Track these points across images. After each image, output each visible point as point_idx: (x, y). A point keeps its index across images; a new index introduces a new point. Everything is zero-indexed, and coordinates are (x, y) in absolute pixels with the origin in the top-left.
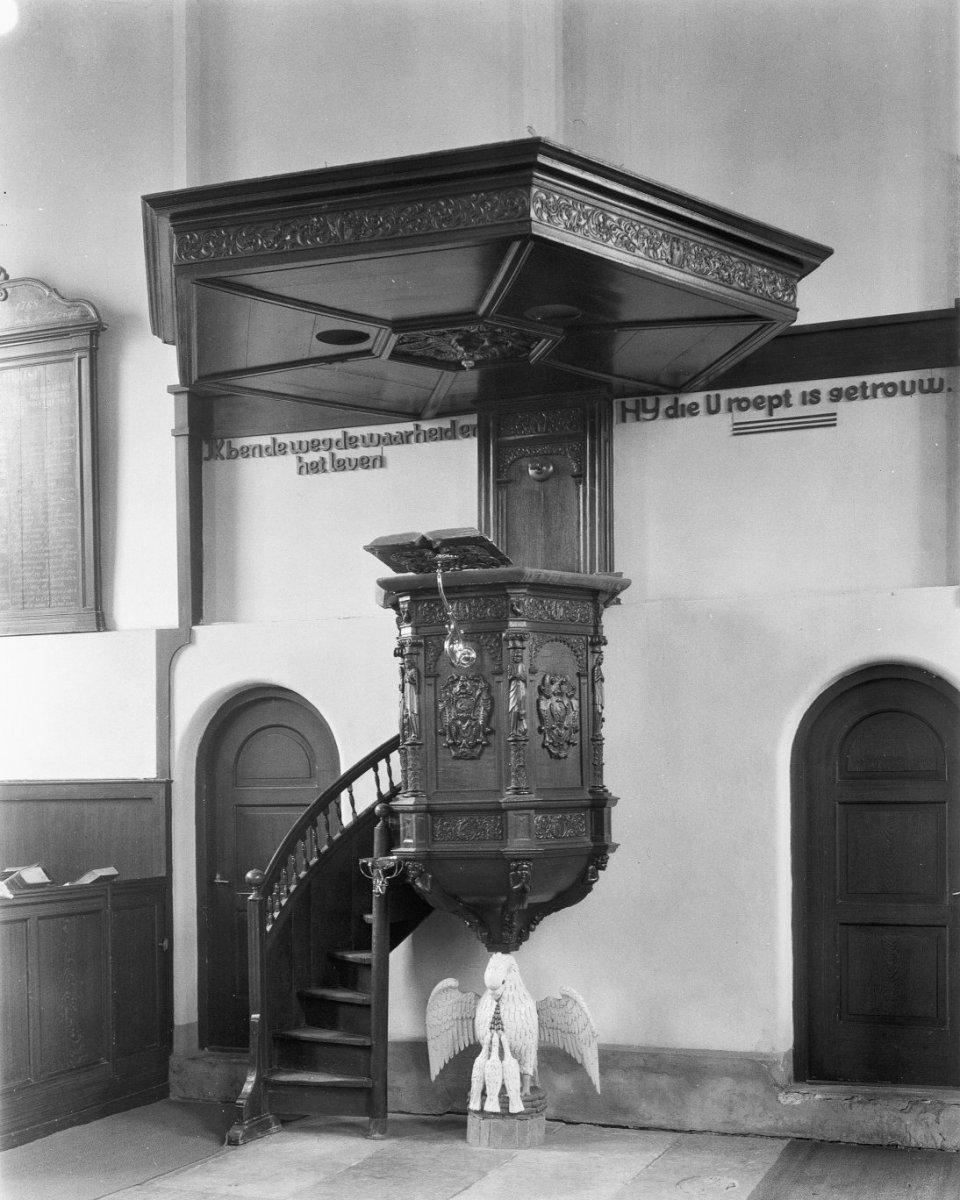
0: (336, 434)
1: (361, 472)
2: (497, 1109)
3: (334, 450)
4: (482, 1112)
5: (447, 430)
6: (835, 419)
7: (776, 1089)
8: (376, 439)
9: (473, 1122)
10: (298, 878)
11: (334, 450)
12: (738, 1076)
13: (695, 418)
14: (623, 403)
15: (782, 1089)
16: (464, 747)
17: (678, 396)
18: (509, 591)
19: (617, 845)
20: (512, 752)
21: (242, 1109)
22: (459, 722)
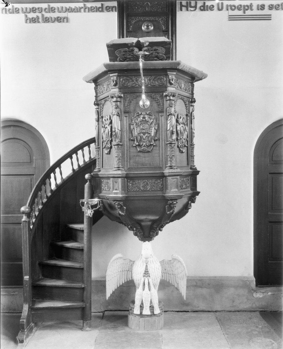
0: (44, 6)
1: (56, 23)
2: (149, 313)
3: (43, 13)
4: (141, 315)
5: (99, 8)
6: (271, 17)
7: (252, 291)
8: (64, 9)
9: (132, 319)
10: (39, 209)
11: (43, 13)
12: (236, 287)
13: (212, 11)
14: (181, 3)
15: (255, 291)
16: (144, 146)
17: (205, 1)
18: (168, 73)
19: (199, 193)
20: (169, 149)
21: (24, 324)
22: (142, 135)
